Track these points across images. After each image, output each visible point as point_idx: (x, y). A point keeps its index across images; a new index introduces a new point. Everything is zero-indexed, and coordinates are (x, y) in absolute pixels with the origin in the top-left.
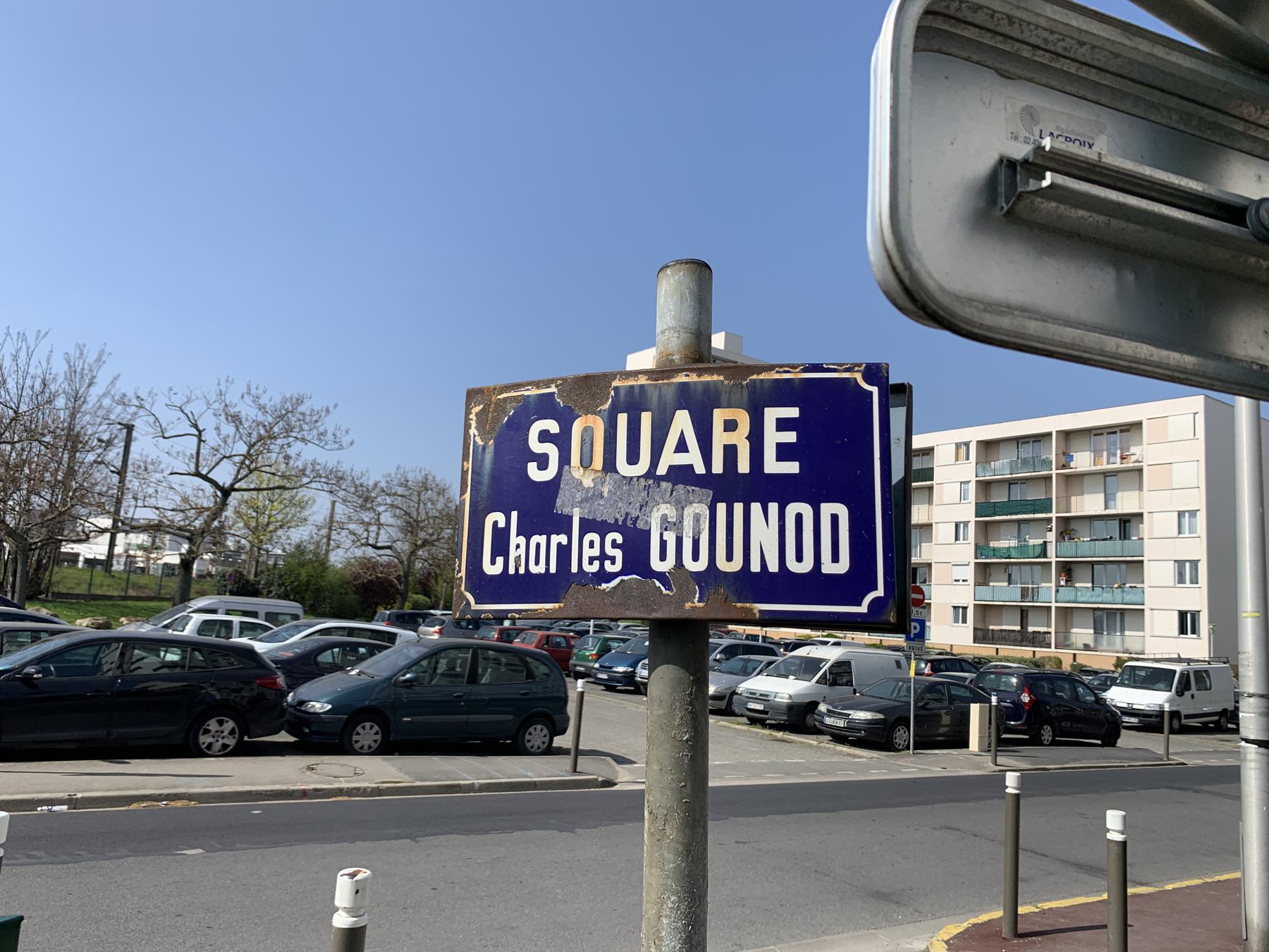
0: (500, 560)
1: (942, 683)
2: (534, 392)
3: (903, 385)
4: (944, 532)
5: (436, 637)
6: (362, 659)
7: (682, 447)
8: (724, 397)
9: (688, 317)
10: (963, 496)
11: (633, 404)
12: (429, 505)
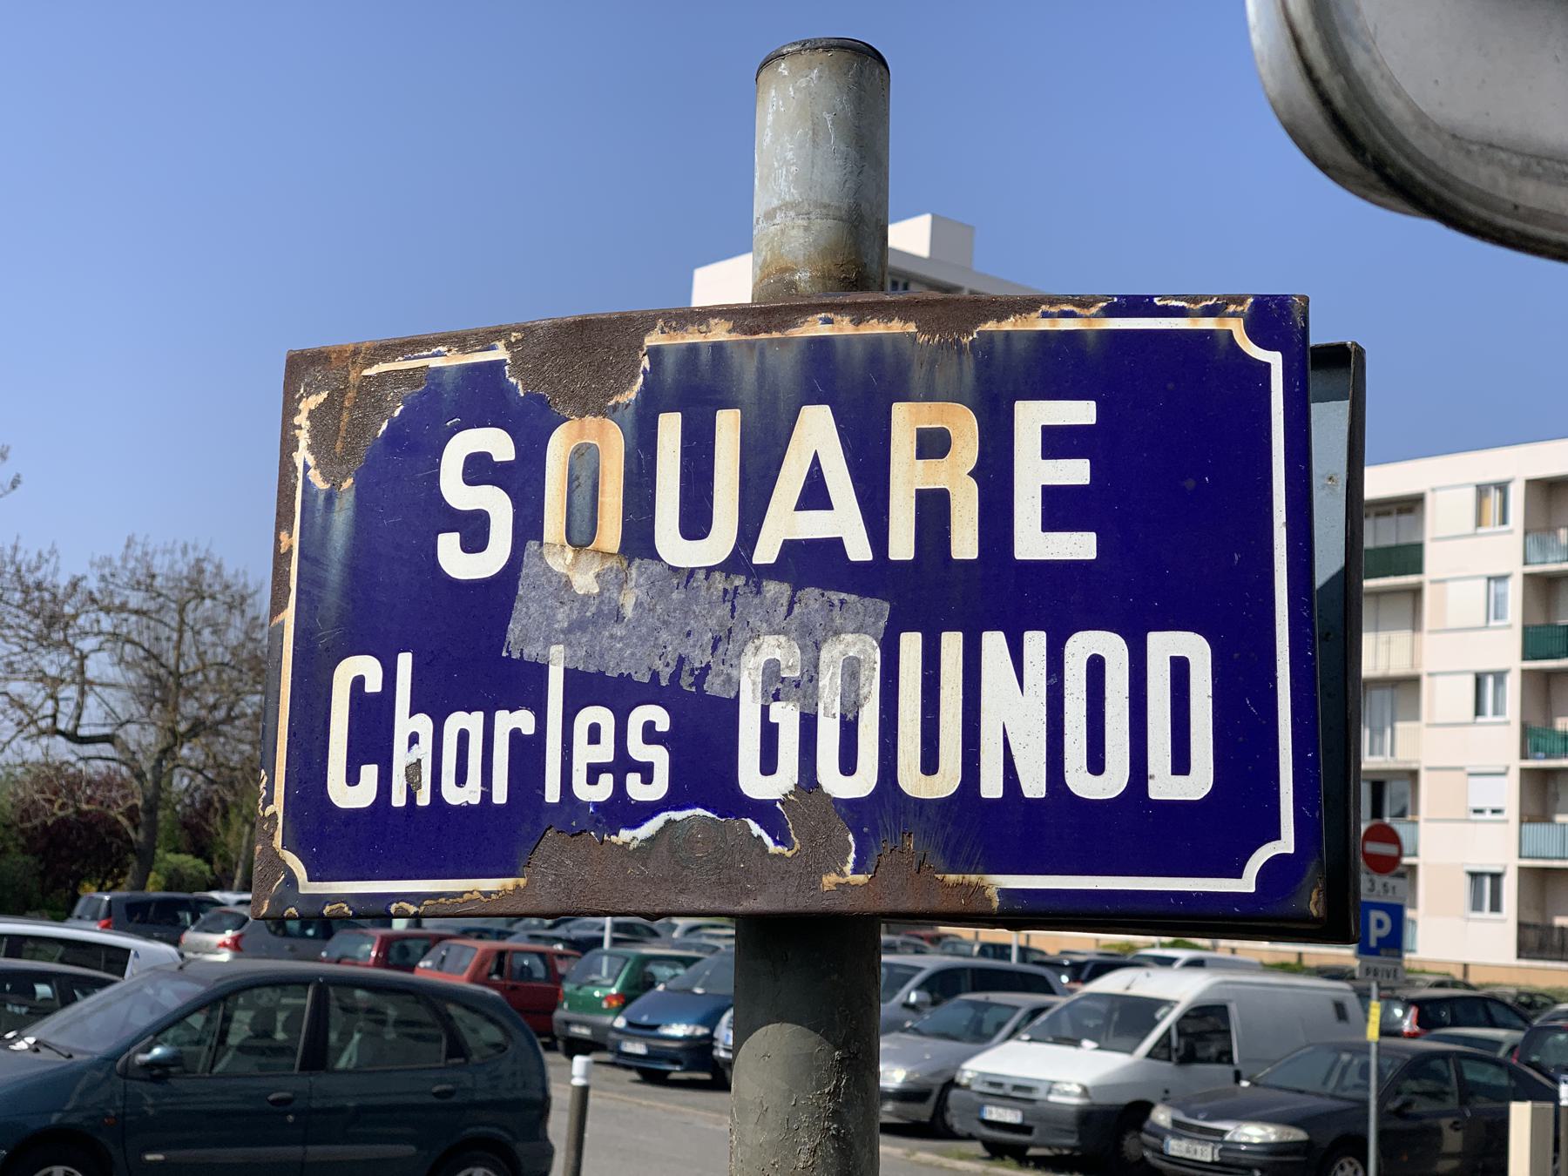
0: (370, 773)
1: (1444, 1055)
2: (451, 360)
3: (1343, 347)
4: (1446, 697)
5: (225, 956)
6: (42, 1011)
7: (815, 495)
8: (918, 375)
9: (831, 178)
10: (1495, 609)
11: (696, 390)
12: (206, 632)
